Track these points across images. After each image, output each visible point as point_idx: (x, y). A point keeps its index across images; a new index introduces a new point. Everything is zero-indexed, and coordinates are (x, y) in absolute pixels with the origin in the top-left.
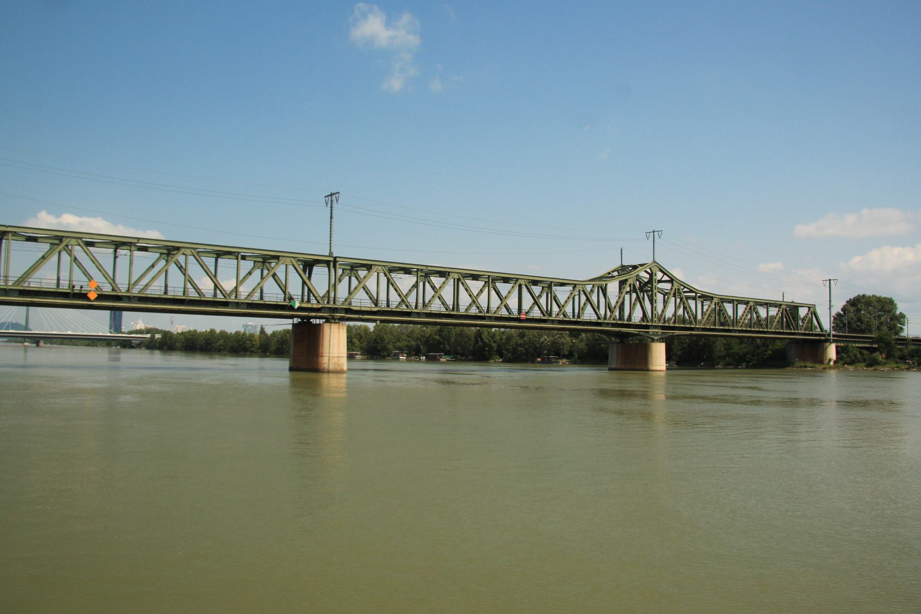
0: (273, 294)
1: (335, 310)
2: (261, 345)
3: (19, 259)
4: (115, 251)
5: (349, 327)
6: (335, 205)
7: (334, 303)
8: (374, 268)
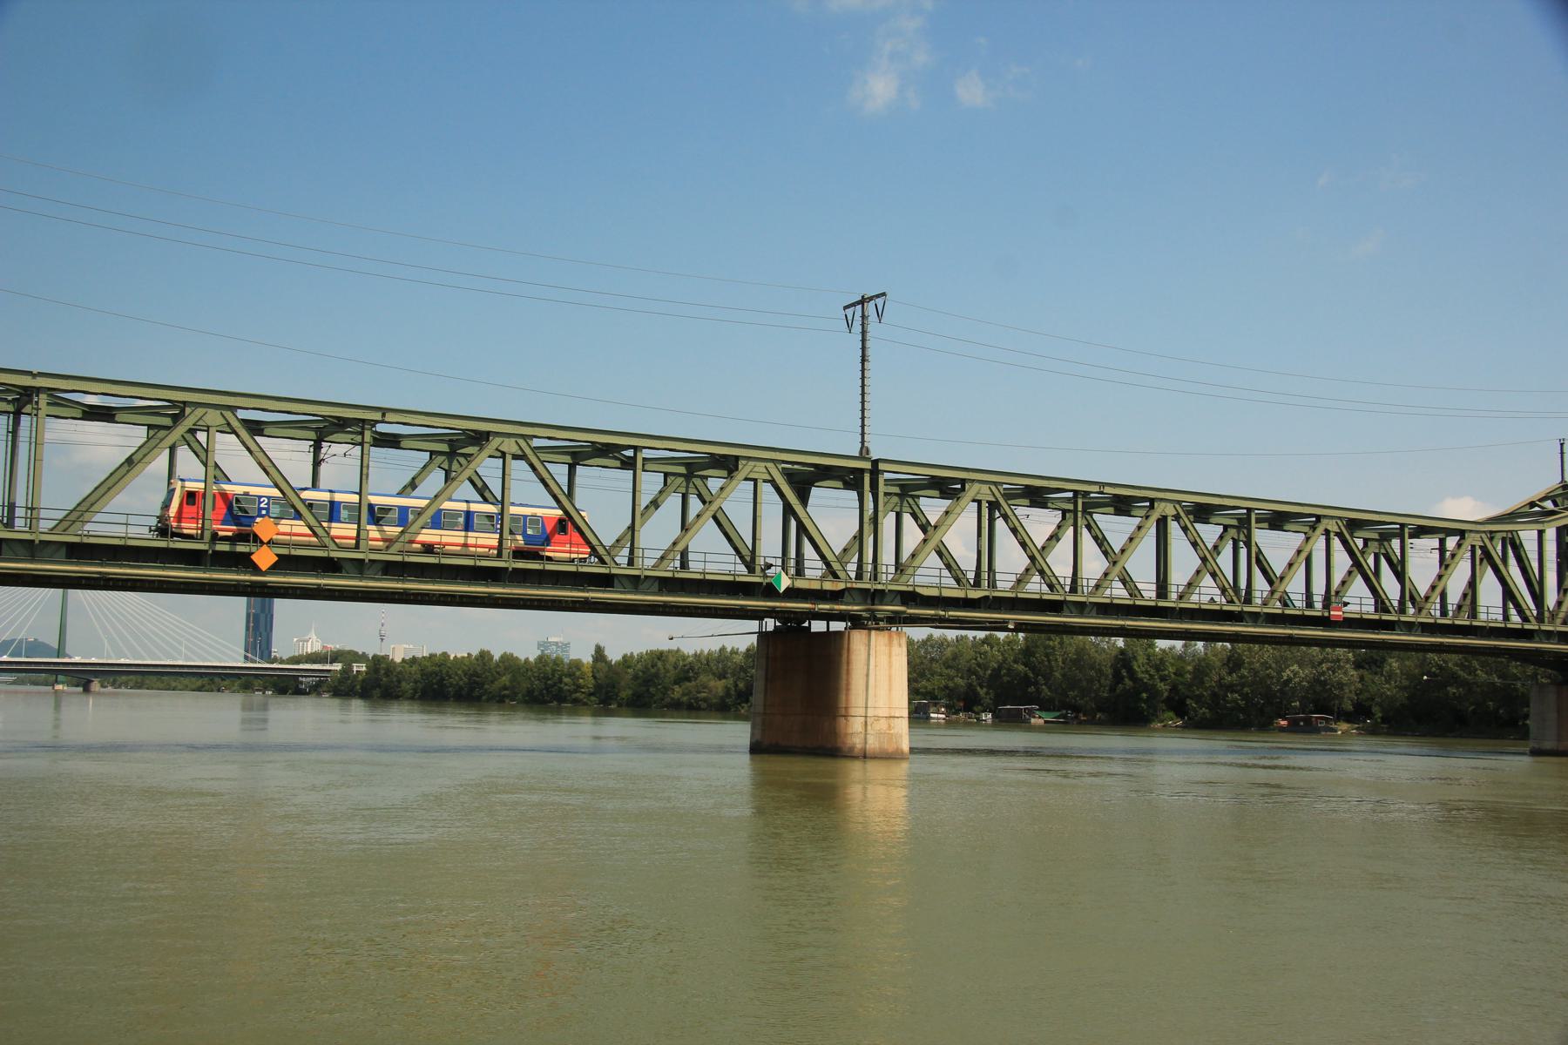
0: (712, 556)
1: (877, 596)
2: (598, 687)
3: (74, 462)
4: (317, 448)
5: (910, 643)
6: (873, 326)
7: (875, 577)
8: (745, 469)
